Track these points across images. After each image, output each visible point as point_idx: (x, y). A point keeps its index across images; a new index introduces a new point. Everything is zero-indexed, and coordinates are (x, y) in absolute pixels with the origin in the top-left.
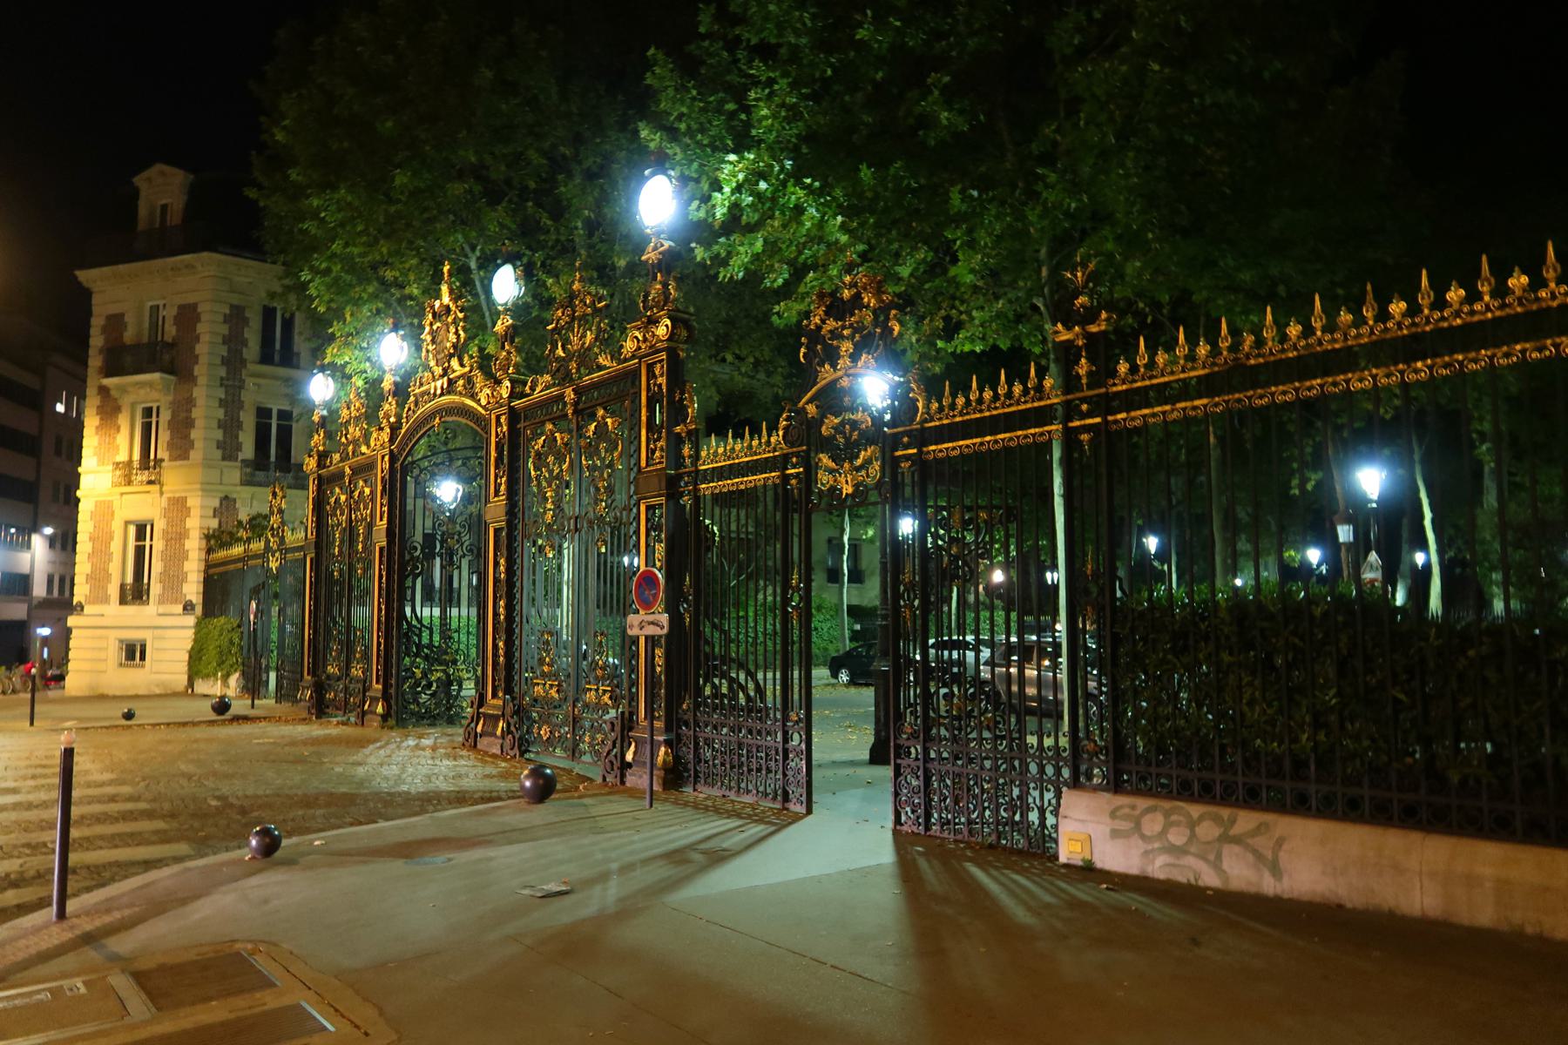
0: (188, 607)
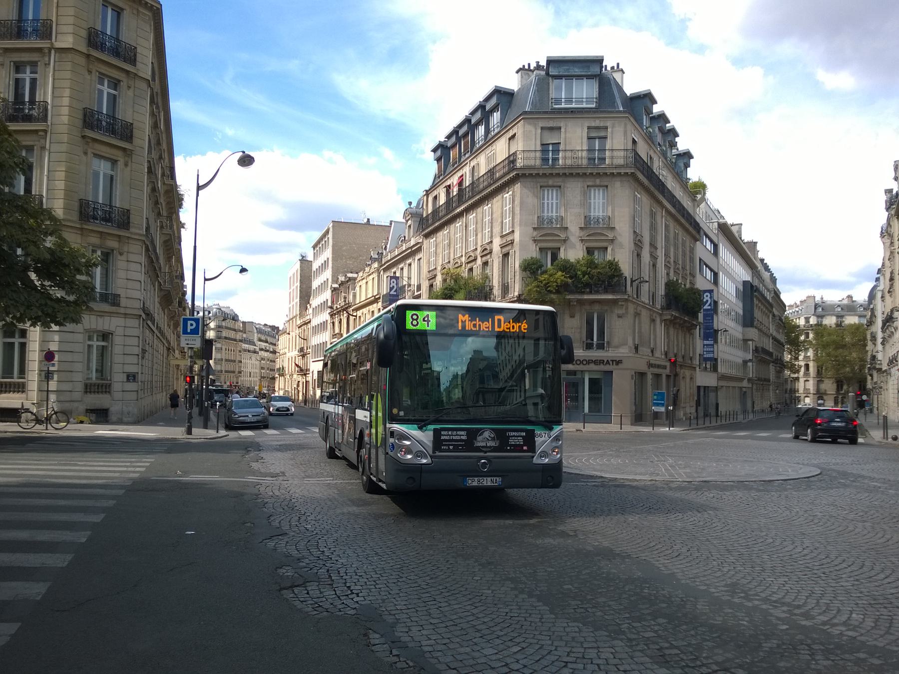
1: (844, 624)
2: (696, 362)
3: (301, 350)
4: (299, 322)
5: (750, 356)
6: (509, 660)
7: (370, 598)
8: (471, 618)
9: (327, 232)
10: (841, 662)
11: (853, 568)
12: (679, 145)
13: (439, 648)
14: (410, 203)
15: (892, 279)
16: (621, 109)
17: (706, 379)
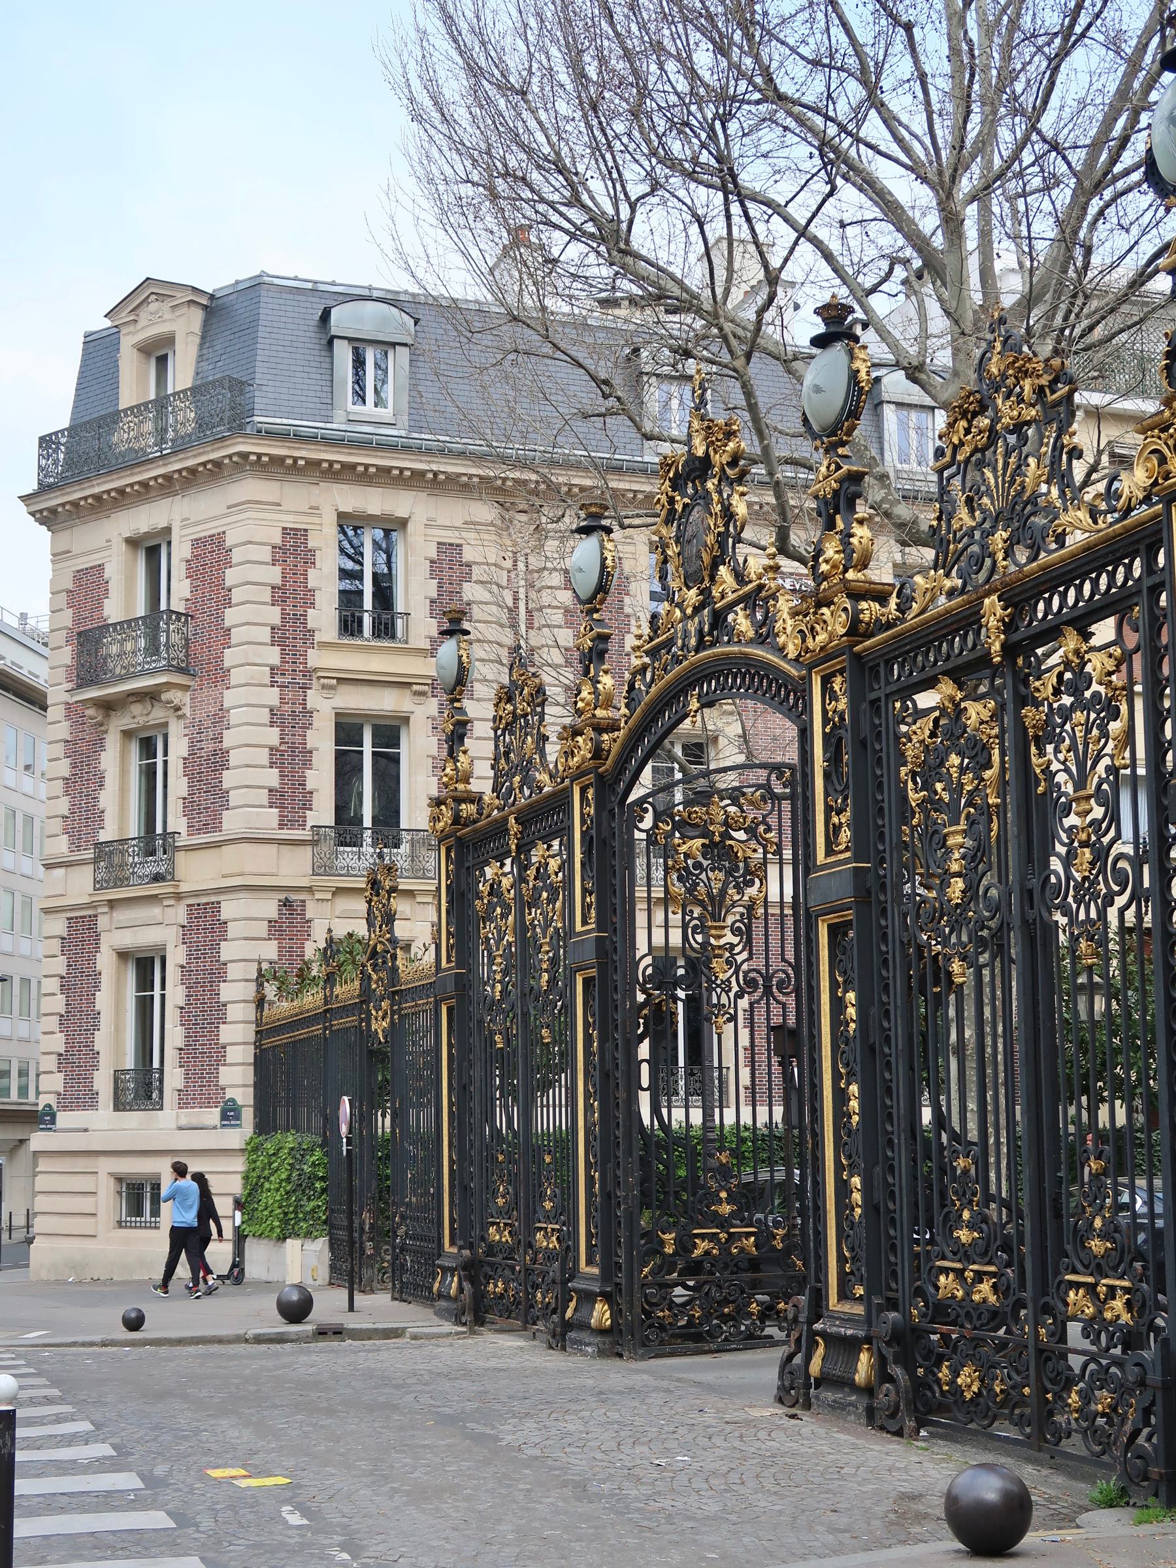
0: (230, 1114)
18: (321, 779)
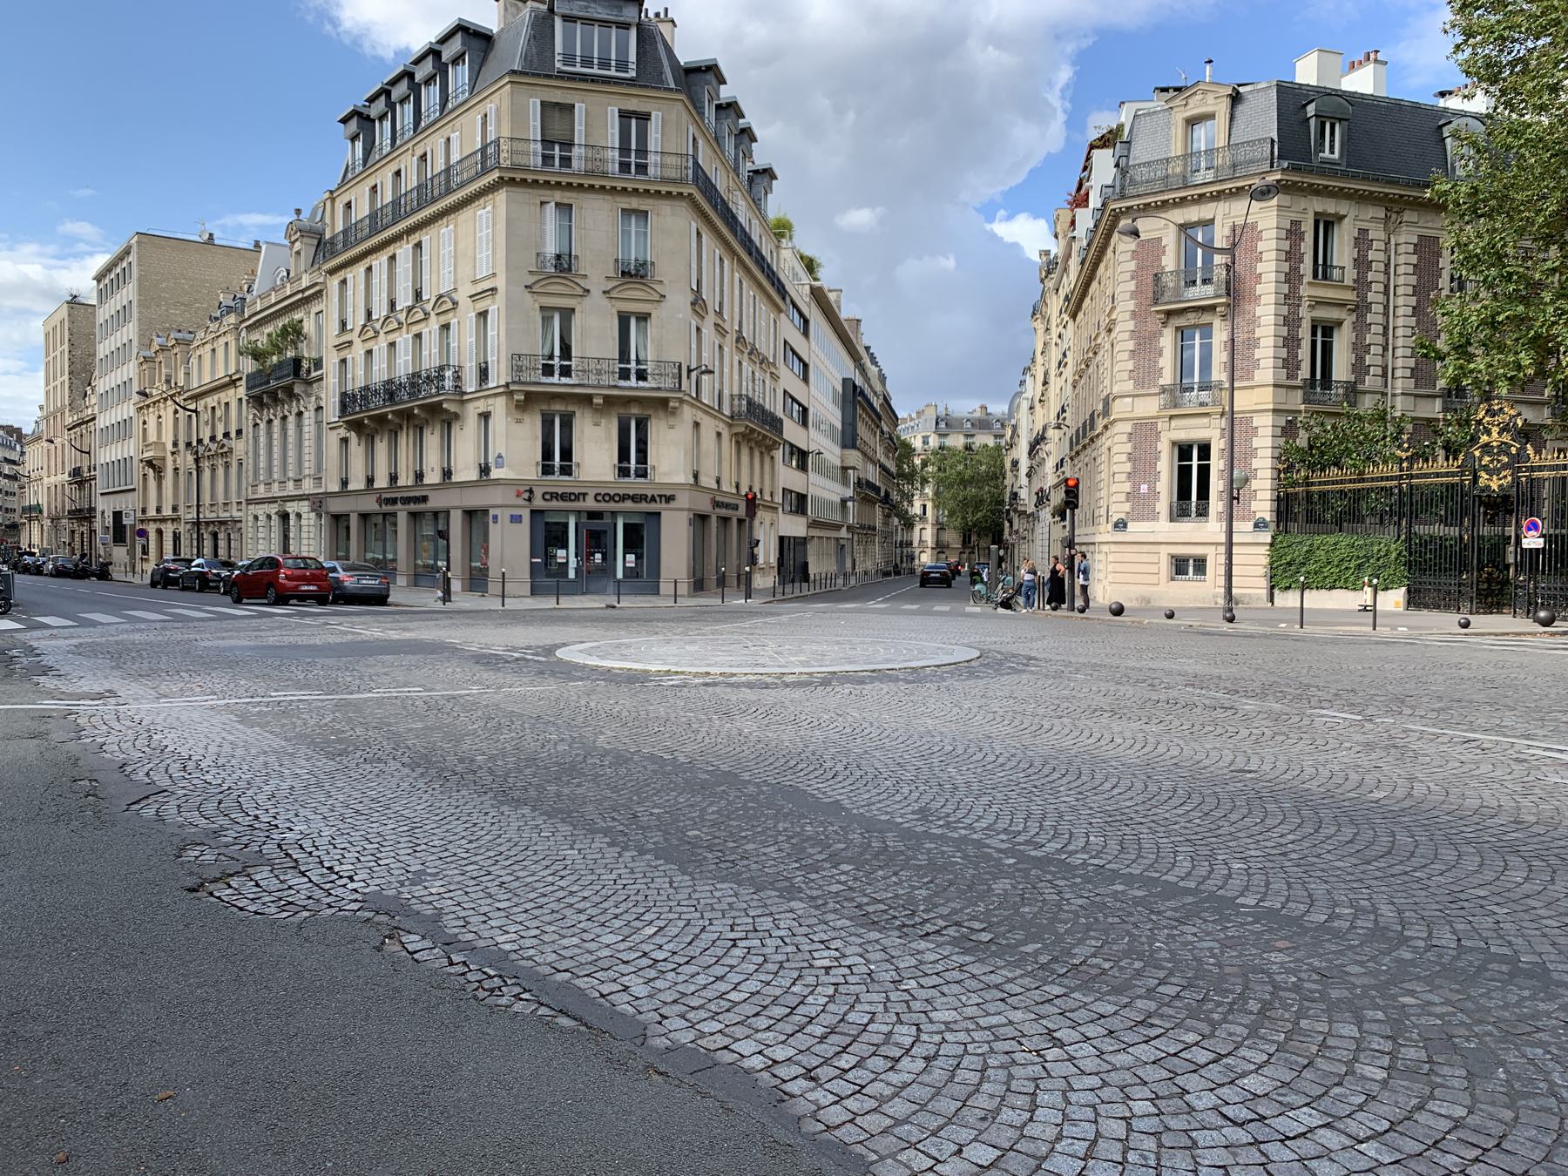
1: (1084, 850)
2: (779, 498)
3: (76, 472)
4: (69, 420)
5: (850, 493)
6: (646, 948)
7: (378, 881)
8: (561, 894)
9: (127, 252)
10: (1098, 899)
11: (1069, 778)
12: (755, 157)
13: (528, 943)
14: (298, 212)
15: (1045, 383)
16: (673, 86)
17: (794, 527)
18: (1304, 353)
